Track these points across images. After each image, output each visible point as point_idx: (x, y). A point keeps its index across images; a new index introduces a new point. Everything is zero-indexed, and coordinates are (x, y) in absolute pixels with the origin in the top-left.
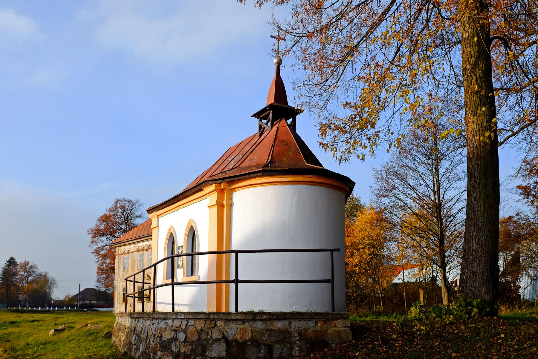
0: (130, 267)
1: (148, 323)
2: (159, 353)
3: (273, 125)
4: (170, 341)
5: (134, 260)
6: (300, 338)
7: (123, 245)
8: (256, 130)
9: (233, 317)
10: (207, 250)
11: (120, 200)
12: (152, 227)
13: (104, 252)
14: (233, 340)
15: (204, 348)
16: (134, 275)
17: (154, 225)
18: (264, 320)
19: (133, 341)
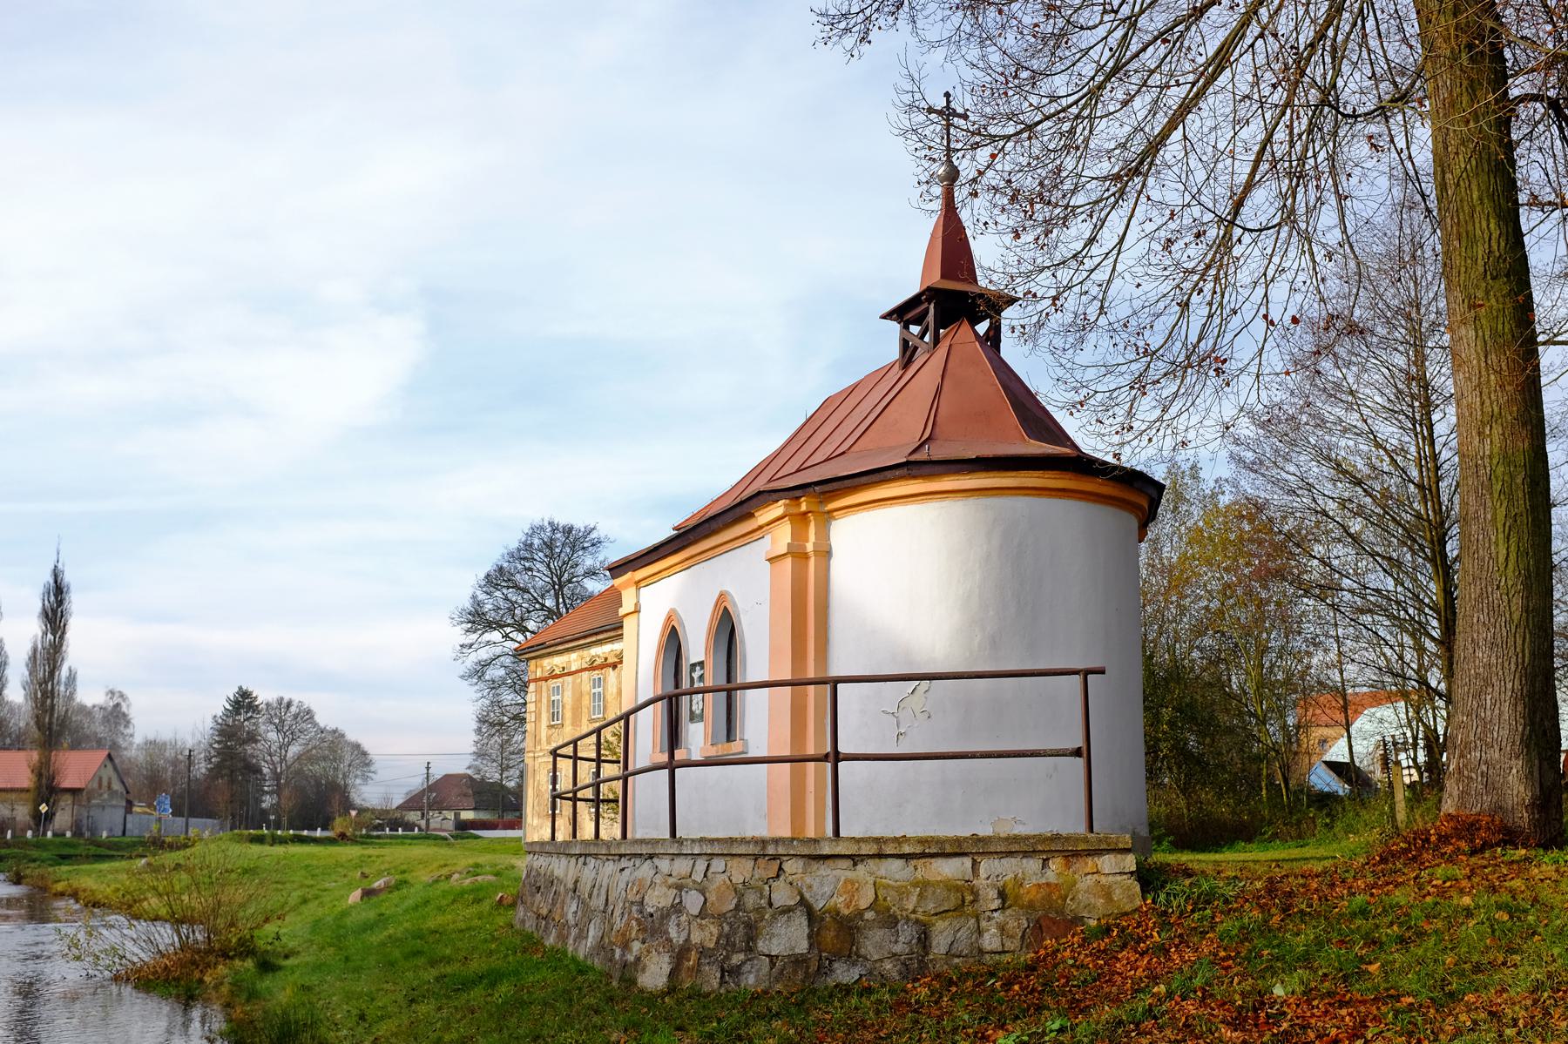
0: (568, 714)
1: (610, 867)
2: (636, 946)
3: (937, 340)
4: (665, 915)
5: (578, 698)
6: (1004, 902)
7: (549, 654)
8: (894, 353)
9: (826, 851)
10: (766, 678)
11: (542, 528)
12: (622, 612)
13: (496, 672)
14: (824, 911)
15: (752, 932)
16: (575, 742)
17: (627, 606)
18: (906, 857)
19: (570, 916)
